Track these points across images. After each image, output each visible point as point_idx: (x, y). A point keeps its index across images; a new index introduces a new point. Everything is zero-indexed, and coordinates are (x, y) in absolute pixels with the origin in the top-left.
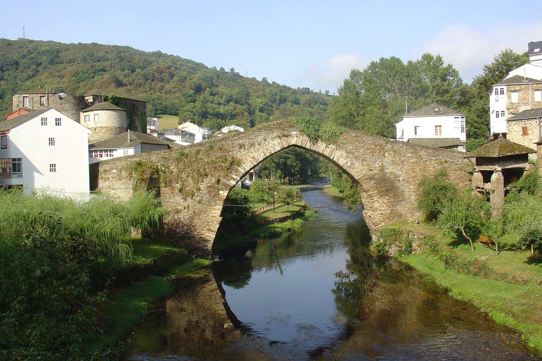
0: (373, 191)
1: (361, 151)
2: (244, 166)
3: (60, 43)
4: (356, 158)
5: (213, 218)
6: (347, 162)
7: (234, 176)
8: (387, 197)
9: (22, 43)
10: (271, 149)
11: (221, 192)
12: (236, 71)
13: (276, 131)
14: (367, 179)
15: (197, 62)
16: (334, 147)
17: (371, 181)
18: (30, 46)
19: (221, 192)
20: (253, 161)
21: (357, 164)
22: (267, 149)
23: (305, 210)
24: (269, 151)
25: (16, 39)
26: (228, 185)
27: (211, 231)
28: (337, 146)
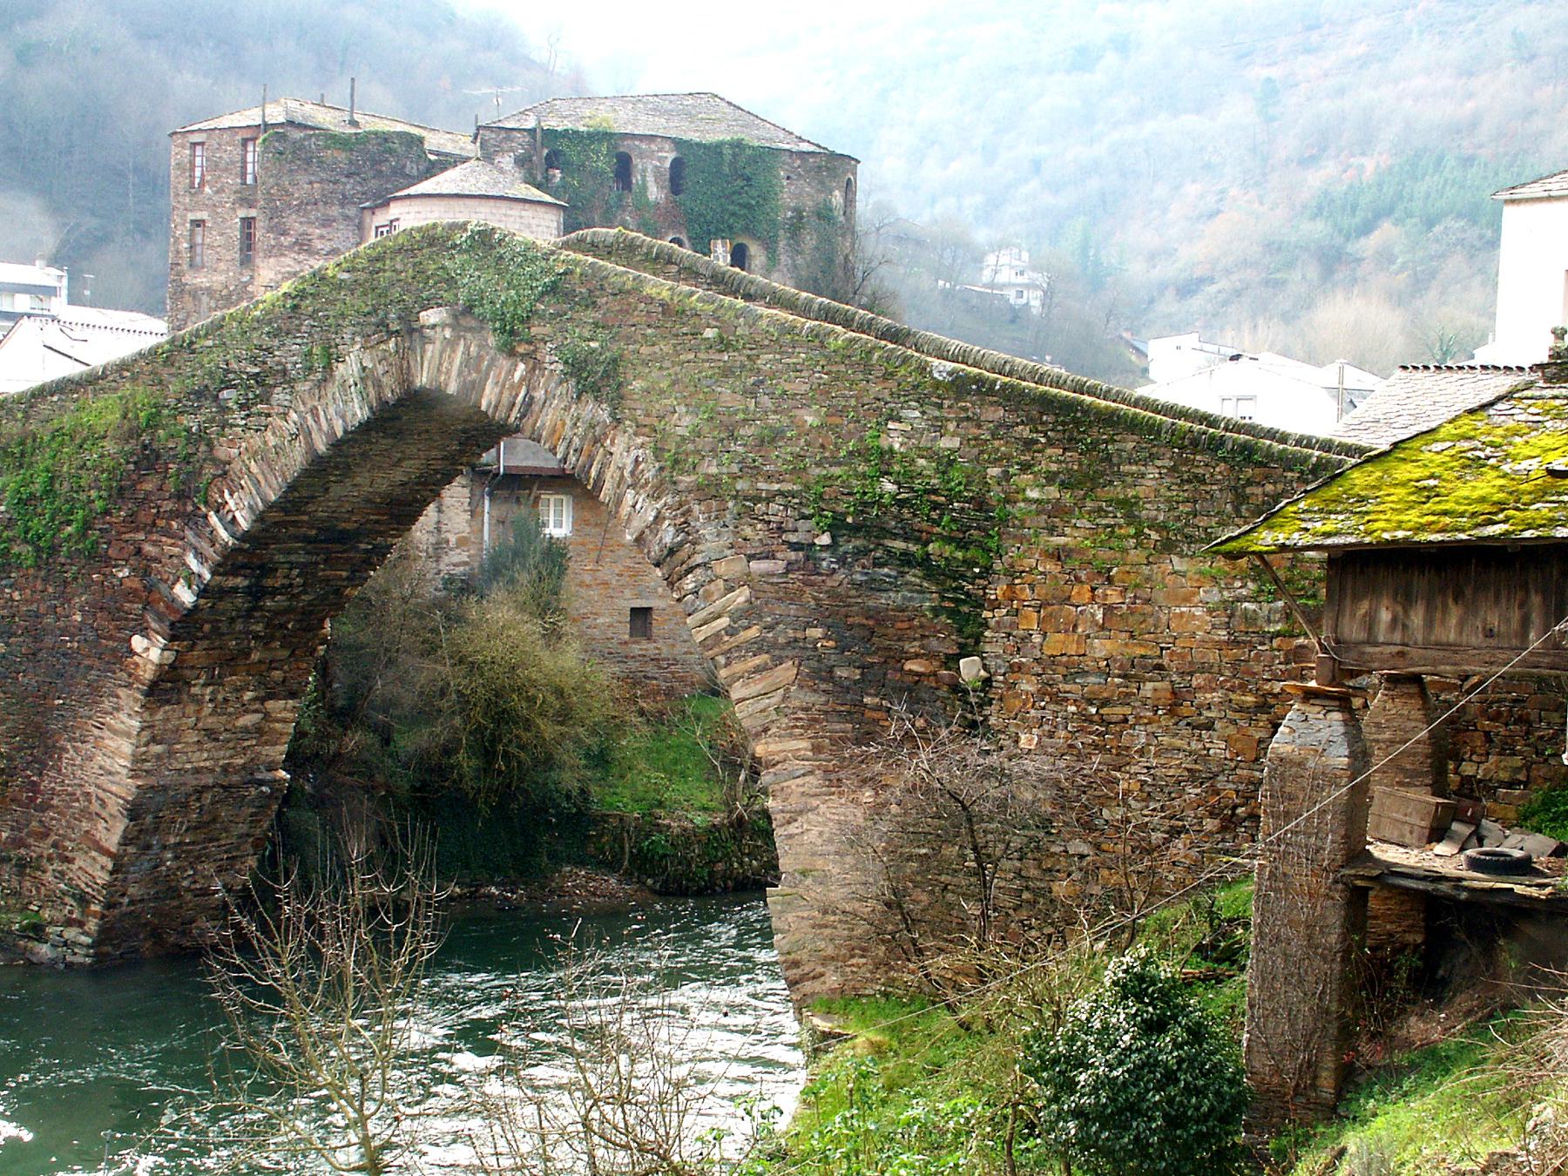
11: (138, 642)
19: (138, 642)
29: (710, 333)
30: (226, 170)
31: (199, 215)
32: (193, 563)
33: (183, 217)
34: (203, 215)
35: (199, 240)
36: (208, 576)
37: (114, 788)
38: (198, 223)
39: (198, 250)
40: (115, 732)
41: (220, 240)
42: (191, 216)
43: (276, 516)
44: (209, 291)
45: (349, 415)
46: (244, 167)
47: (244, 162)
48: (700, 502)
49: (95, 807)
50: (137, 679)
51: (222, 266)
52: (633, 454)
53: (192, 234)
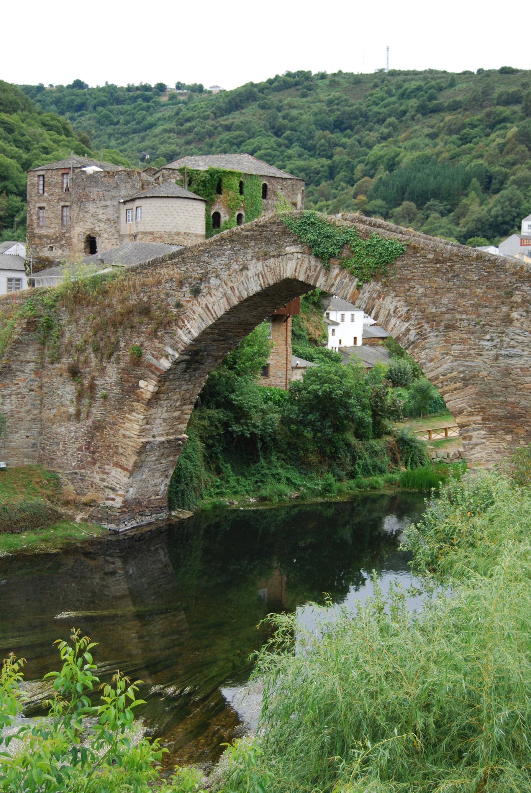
0: (471, 414)
1: (445, 301)
2: (189, 326)
3: (445, 72)
4: (432, 319)
5: (126, 441)
6: (408, 330)
7: (170, 351)
8: (509, 437)
9: (383, 78)
10: (241, 288)
11: (142, 383)
12: (110, 83)
13: (252, 243)
14: (454, 380)
15: (226, 76)
16: (378, 287)
17: (466, 385)
18: (394, 80)
19: (142, 383)
20: (204, 316)
21: (432, 338)
22: (232, 288)
23: (71, 416)
24: (237, 293)
25: (373, 72)
26: (157, 369)
27: (122, 467)
28: (385, 285)
29: (431, 256)
30: (55, 186)
31: (42, 205)
32: (170, 351)
33: (34, 206)
34: (44, 205)
35: (41, 215)
36: (177, 356)
37: (130, 443)
38: (41, 208)
39: (41, 219)
40: (131, 420)
41: (52, 215)
42: (38, 205)
43: (209, 330)
44: (47, 237)
45: (250, 289)
46: (62, 185)
47: (63, 183)
48: (428, 323)
49: (121, 450)
50: (142, 399)
51: (53, 226)
52: (394, 304)
53: (38, 212)
